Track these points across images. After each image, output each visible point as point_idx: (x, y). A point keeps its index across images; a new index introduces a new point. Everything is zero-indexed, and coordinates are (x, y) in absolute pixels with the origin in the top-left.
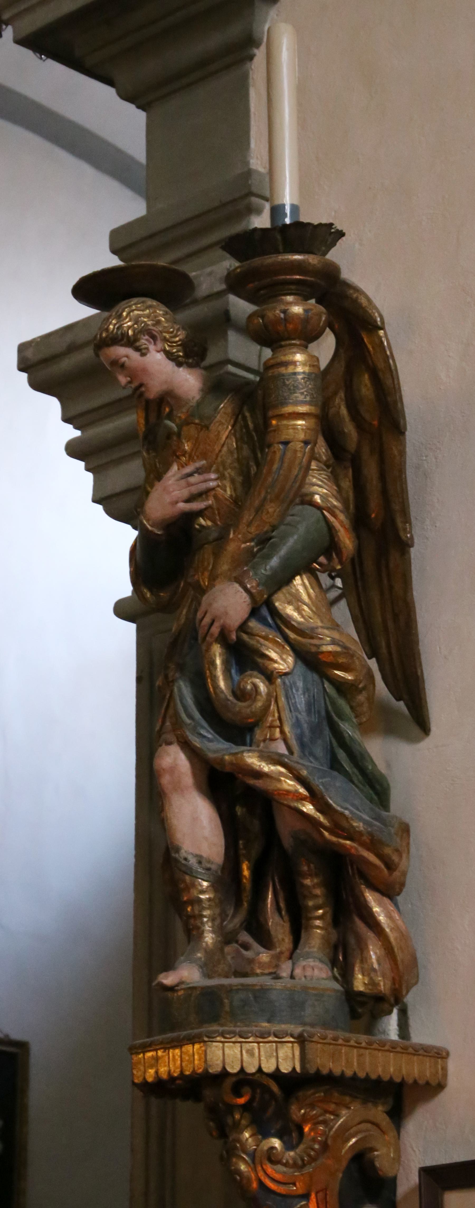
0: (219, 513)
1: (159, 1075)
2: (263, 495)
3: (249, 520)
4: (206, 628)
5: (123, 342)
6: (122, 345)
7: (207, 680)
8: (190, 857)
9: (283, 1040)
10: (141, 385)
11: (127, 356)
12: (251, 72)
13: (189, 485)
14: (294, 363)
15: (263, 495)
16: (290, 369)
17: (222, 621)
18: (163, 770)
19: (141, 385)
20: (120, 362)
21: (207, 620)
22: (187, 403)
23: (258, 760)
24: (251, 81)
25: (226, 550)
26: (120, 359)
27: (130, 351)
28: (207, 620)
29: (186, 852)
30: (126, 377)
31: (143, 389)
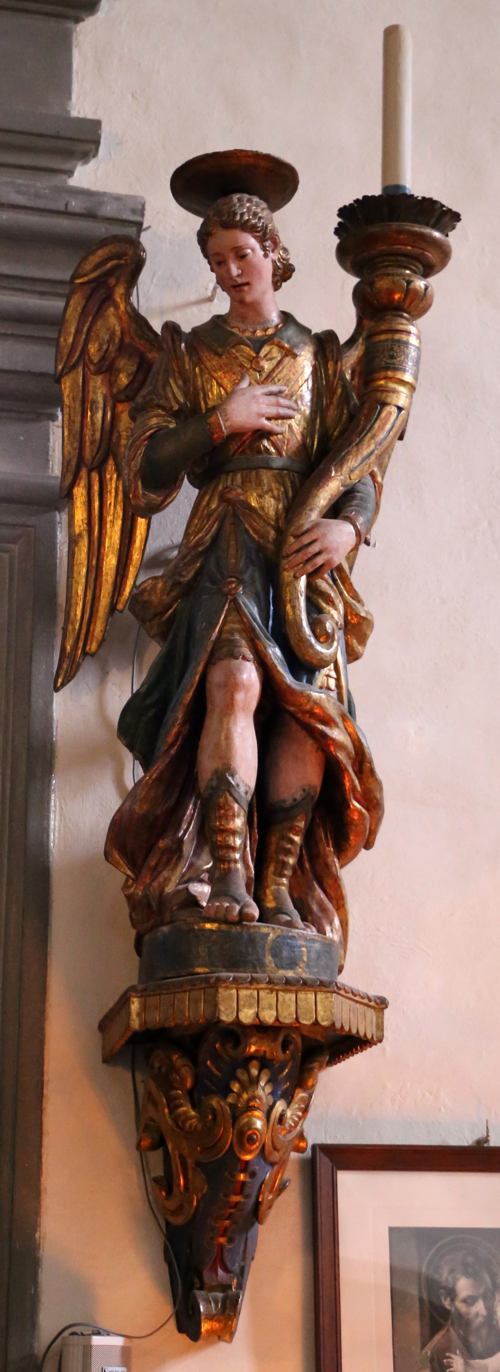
0: (288, 444)
2: (372, 447)
5: (258, 234)
8: (241, 785)
10: (247, 284)
11: (253, 250)
12: (74, 34)
13: (279, 405)
14: (409, 333)
15: (372, 447)
16: (404, 337)
17: (331, 556)
19: (247, 284)
20: (245, 250)
22: (265, 322)
24: (74, 43)
25: (328, 486)
26: (247, 248)
29: (240, 778)
30: (238, 268)
31: (246, 288)
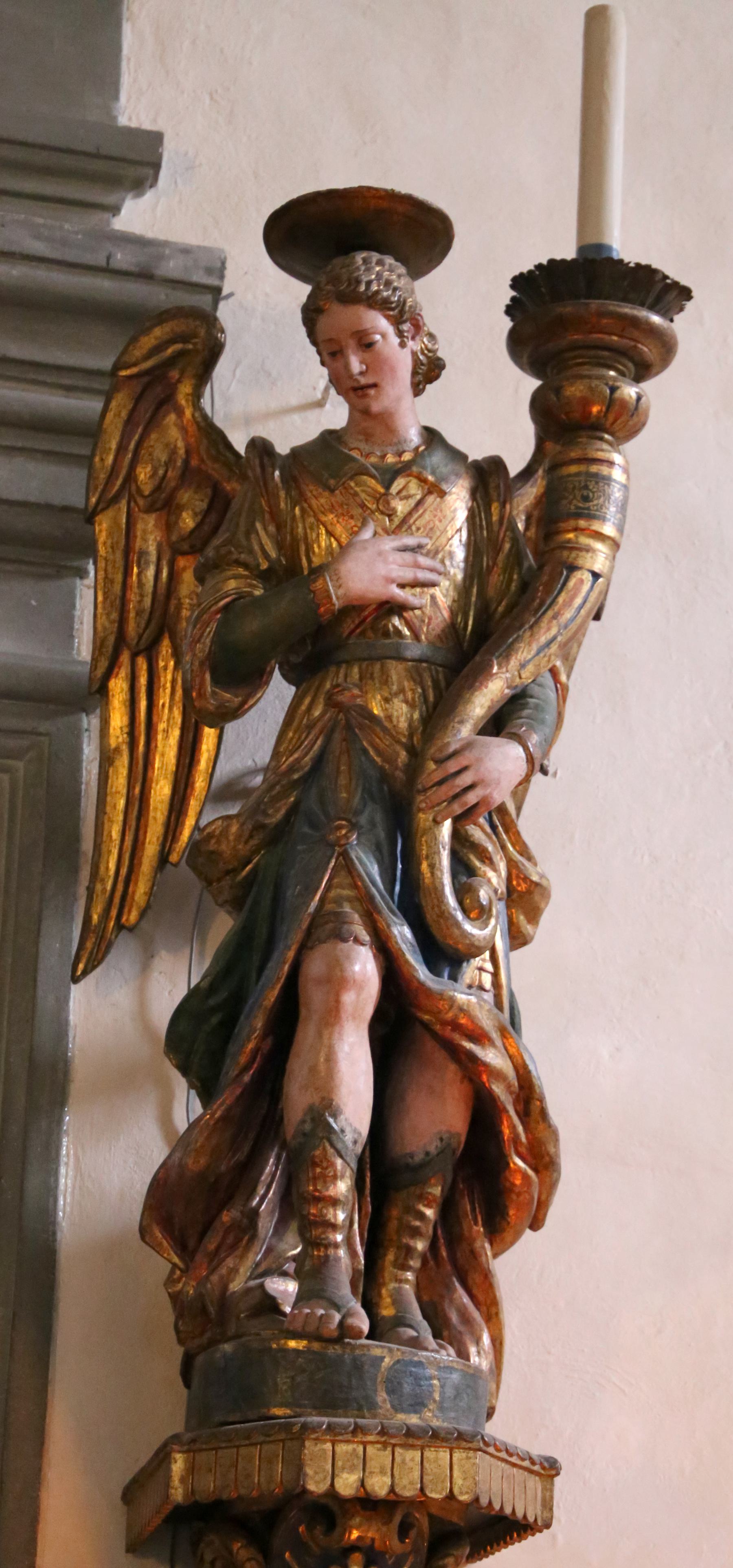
1: (368, 1488)
2: (554, 631)
3: (527, 659)
4: (458, 790)
6: (388, 317)
7: (420, 864)
8: (348, 1130)
9: (271, 1439)
10: (375, 386)
11: (384, 336)
15: (554, 631)
17: (488, 791)
18: (354, 981)
19: (375, 386)
21: (466, 779)
23: (419, 1007)
25: (486, 687)
27: (390, 330)
28: (466, 779)
29: (346, 1119)
31: (372, 392)
